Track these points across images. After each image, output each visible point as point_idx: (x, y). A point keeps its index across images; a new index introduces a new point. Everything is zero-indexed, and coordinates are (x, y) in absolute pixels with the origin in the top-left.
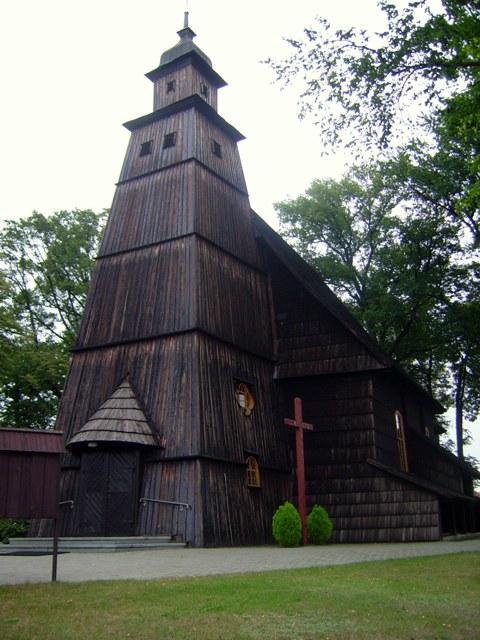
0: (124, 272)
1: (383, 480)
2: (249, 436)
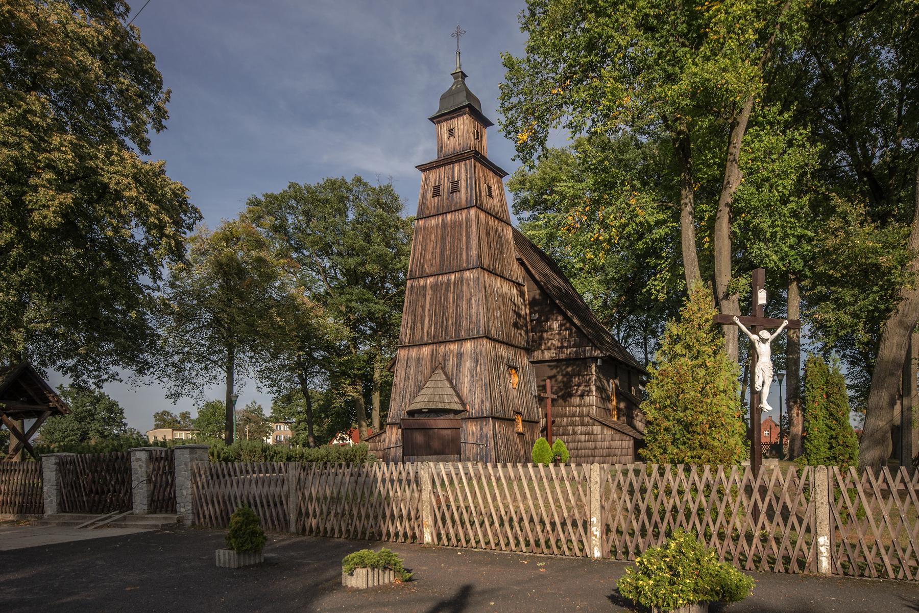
0: (429, 293)
1: (599, 427)
2: (516, 401)
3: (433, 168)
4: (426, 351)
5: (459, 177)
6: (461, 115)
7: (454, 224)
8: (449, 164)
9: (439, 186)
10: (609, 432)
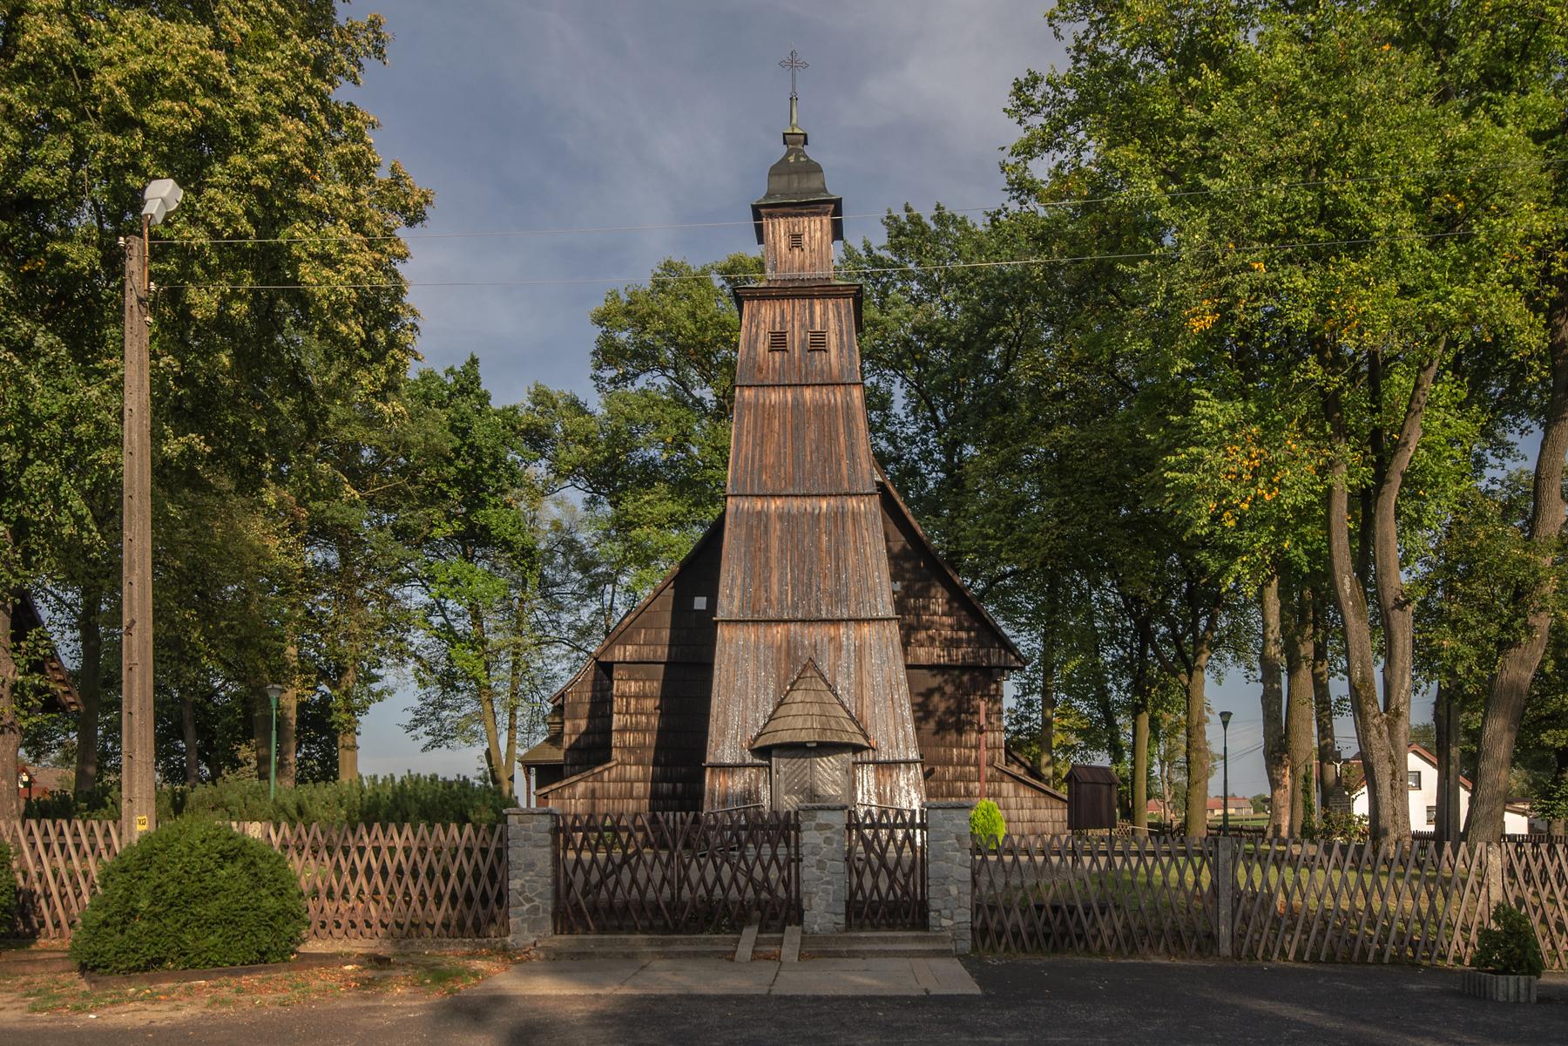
0: (776, 528)
3: (770, 297)
4: (778, 632)
5: (825, 324)
6: (818, 214)
7: (819, 408)
8: (803, 297)
9: (783, 334)
10: (1028, 794)
